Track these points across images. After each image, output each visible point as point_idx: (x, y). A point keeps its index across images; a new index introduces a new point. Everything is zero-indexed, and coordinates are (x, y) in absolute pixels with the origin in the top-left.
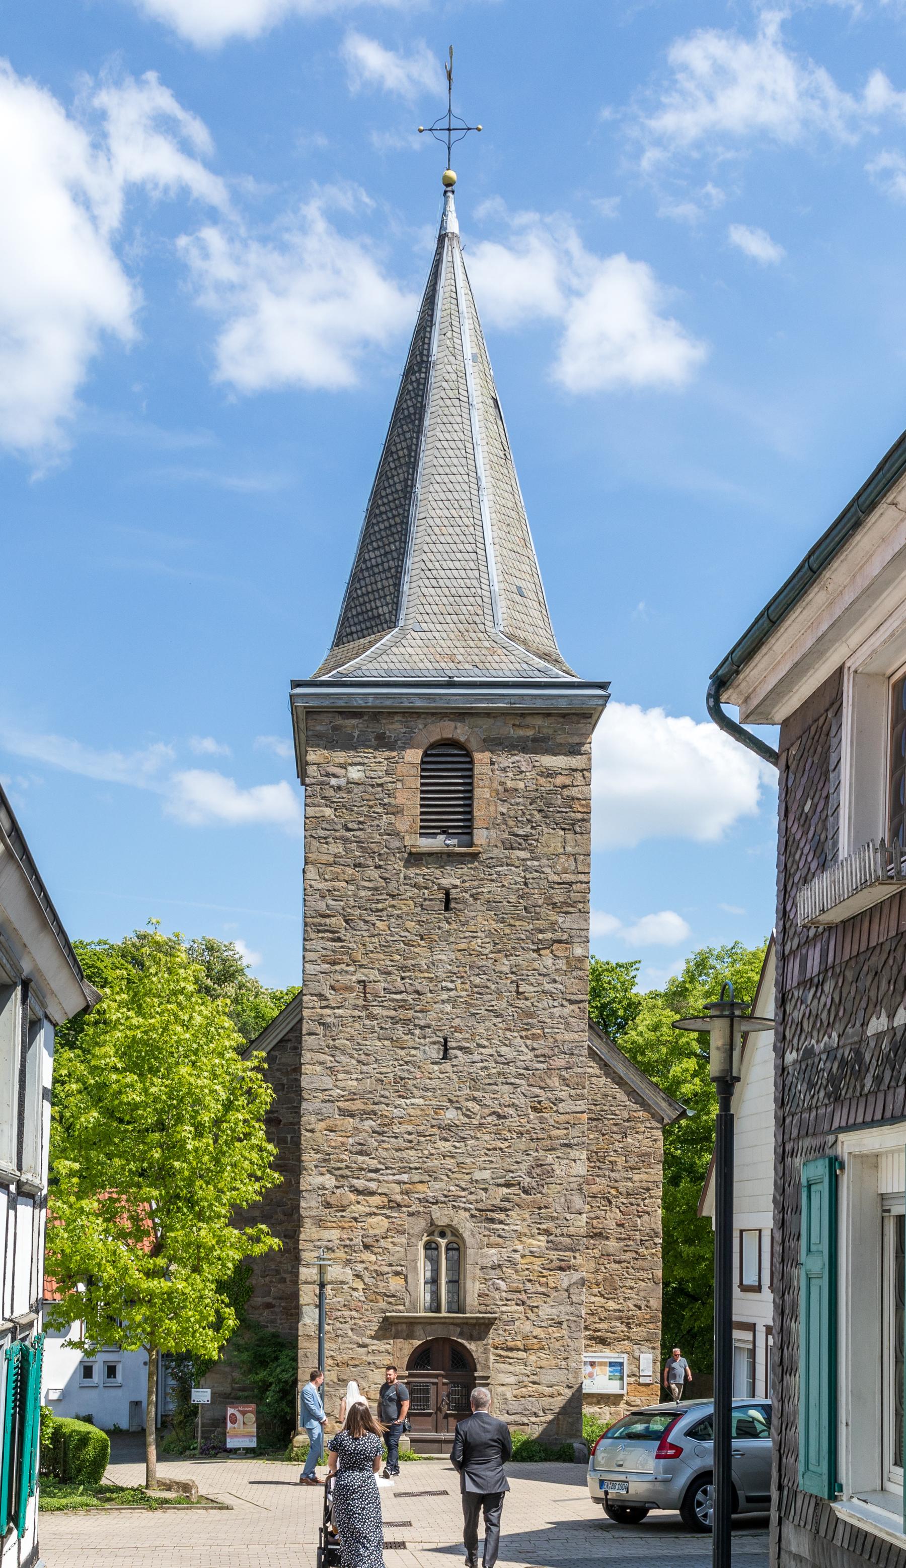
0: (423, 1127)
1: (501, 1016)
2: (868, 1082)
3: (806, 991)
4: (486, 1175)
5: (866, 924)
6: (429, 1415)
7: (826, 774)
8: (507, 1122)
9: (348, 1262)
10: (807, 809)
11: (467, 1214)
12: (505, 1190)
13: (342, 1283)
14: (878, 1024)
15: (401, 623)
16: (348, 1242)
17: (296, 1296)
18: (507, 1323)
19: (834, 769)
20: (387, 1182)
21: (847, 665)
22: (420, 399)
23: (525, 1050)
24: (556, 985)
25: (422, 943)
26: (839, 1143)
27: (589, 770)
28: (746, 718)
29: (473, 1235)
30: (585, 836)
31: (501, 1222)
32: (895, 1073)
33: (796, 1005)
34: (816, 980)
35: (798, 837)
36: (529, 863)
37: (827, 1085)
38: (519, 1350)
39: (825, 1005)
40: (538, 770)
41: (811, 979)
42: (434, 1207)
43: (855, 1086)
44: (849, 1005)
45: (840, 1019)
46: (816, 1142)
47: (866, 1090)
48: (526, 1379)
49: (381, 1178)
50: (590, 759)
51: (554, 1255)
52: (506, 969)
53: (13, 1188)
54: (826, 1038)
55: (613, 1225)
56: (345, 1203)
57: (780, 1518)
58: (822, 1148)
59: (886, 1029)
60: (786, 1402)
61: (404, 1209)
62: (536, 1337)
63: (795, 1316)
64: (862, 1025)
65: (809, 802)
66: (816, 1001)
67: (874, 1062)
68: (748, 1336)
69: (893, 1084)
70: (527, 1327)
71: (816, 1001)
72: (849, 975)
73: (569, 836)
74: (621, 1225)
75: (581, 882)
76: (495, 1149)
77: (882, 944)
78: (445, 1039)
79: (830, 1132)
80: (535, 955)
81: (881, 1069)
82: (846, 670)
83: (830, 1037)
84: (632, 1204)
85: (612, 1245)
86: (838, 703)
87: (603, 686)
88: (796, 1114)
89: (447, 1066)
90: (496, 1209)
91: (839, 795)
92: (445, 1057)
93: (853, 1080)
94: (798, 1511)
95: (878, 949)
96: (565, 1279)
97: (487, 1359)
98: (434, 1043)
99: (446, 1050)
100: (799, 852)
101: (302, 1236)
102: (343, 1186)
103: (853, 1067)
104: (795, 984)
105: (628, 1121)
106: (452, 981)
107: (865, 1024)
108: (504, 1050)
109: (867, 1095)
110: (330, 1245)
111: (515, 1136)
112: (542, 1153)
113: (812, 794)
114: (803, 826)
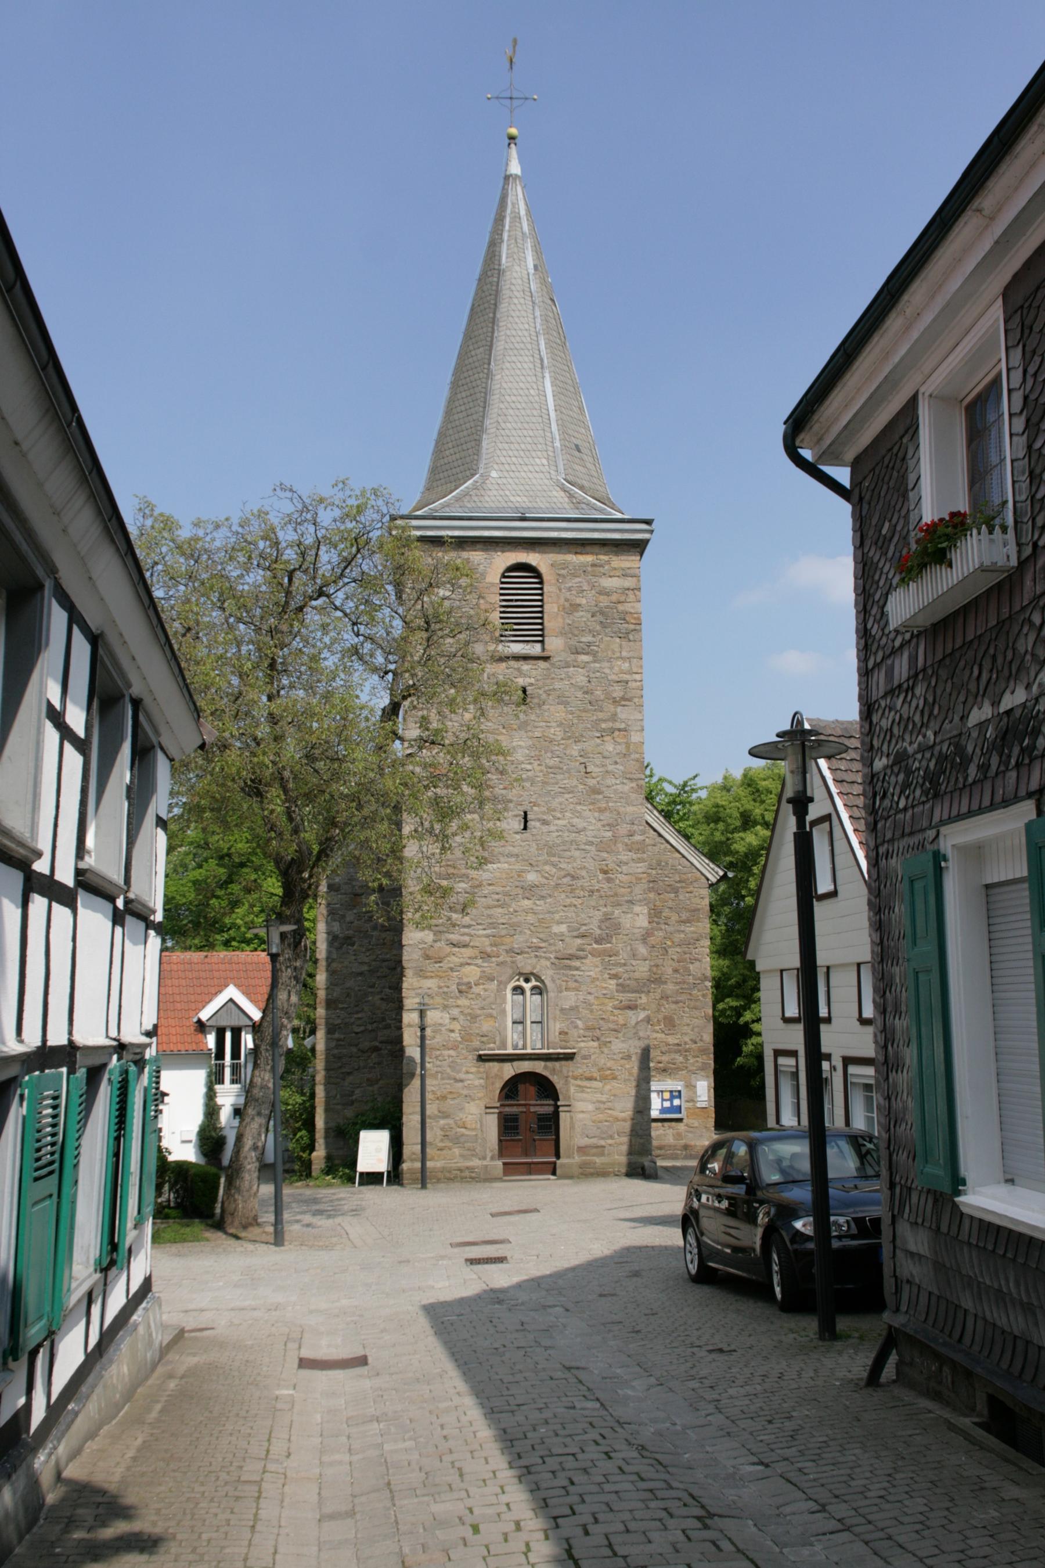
0: (508, 888)
1: (572, 792)
2: (972, 771)
3: (895, 699)
4: (563, 928)
5: (961, 621)
6: (520, 1140)
7: (905, 496)
8: (580, 883)
9: (445, 1007)
10: (884, 532)
11: (548, 963)
12: (579, 941)
13: (440, 1024)
14: (976, 716)
15: (481, 471)
16: (446, 990)
17: (399, 1039)
18: (585, 1057)
19: (913, 488)
20: (478, 936)
21: (922, 390)
22: (486, 366)
23: (594, 821)
24: (618, 766)
25: (504, 731)
26: (941, 837)
27: (639, 589)
29: (553, 981)
30: (638, 644)
31: (577, 969)
32: (1004, 758)
33: (883, 713)
34: (905, 686)
35: (875, 560)
36: (592, 665)
37: (924, 783)
38: (596, 1080)
39: (917, 707)
40: (598, 589)
41: (900, 686)
42: (519, 957)
43: (957, 779)
45: (936, 717)
47: (970, 780)
48: (602, 1106)
49: (473, 932)
50: (639, 581)
51: (622, 996)
52: (575, 753)
53: (120, 903)
54: (920, 738)
55: (670, 971)
56: (442, 955)
57: (893, 1216)
58: (921, 846)
59: (990, 716)
60: (893, 1099)
61: (494, 959)
62: (610, 1069)
64: (962, 718)
65: (887, 525)
66: (906, 706)
67: (978, 751)
68: (791, 1061)
69: (1002, 768)
70: (602, 1061)
71: (906, 706)
74: (676, 971)
75: (636, 681)
76: (570, 906)
77: (980, 636)
78: (525, 813)
79: (930, 827)
80: (598, 741)
81: (987, 756)
82: (920, 396)
83: (924, 736)
84: (685, 953)
85: (670, 987)
86: (915, 427)
87: (648, 522)
88: (889, 817)
89: (527, 835)
90: (570, 957)
91: (920, 510)
92: (525, 828)
93: (954, 773)
94: (914, 1209)
95: (976, 643)
96: (634, 1017)
97: (568, 1090)
98: (516, 816)
99: (526, 822)
100: (878, 573)
101: (405, 985)
102: (440, 940)
103: (954, 759)
104: (881, 694)
105: (680, 882)
106: (530, 763)
107: (964, 718)
108: (575, 821)
109: (971, 785)
110: (430, 992)
111: (587, 894)
112: (609, 909)
113: (889, 516)
114: (881, 548)
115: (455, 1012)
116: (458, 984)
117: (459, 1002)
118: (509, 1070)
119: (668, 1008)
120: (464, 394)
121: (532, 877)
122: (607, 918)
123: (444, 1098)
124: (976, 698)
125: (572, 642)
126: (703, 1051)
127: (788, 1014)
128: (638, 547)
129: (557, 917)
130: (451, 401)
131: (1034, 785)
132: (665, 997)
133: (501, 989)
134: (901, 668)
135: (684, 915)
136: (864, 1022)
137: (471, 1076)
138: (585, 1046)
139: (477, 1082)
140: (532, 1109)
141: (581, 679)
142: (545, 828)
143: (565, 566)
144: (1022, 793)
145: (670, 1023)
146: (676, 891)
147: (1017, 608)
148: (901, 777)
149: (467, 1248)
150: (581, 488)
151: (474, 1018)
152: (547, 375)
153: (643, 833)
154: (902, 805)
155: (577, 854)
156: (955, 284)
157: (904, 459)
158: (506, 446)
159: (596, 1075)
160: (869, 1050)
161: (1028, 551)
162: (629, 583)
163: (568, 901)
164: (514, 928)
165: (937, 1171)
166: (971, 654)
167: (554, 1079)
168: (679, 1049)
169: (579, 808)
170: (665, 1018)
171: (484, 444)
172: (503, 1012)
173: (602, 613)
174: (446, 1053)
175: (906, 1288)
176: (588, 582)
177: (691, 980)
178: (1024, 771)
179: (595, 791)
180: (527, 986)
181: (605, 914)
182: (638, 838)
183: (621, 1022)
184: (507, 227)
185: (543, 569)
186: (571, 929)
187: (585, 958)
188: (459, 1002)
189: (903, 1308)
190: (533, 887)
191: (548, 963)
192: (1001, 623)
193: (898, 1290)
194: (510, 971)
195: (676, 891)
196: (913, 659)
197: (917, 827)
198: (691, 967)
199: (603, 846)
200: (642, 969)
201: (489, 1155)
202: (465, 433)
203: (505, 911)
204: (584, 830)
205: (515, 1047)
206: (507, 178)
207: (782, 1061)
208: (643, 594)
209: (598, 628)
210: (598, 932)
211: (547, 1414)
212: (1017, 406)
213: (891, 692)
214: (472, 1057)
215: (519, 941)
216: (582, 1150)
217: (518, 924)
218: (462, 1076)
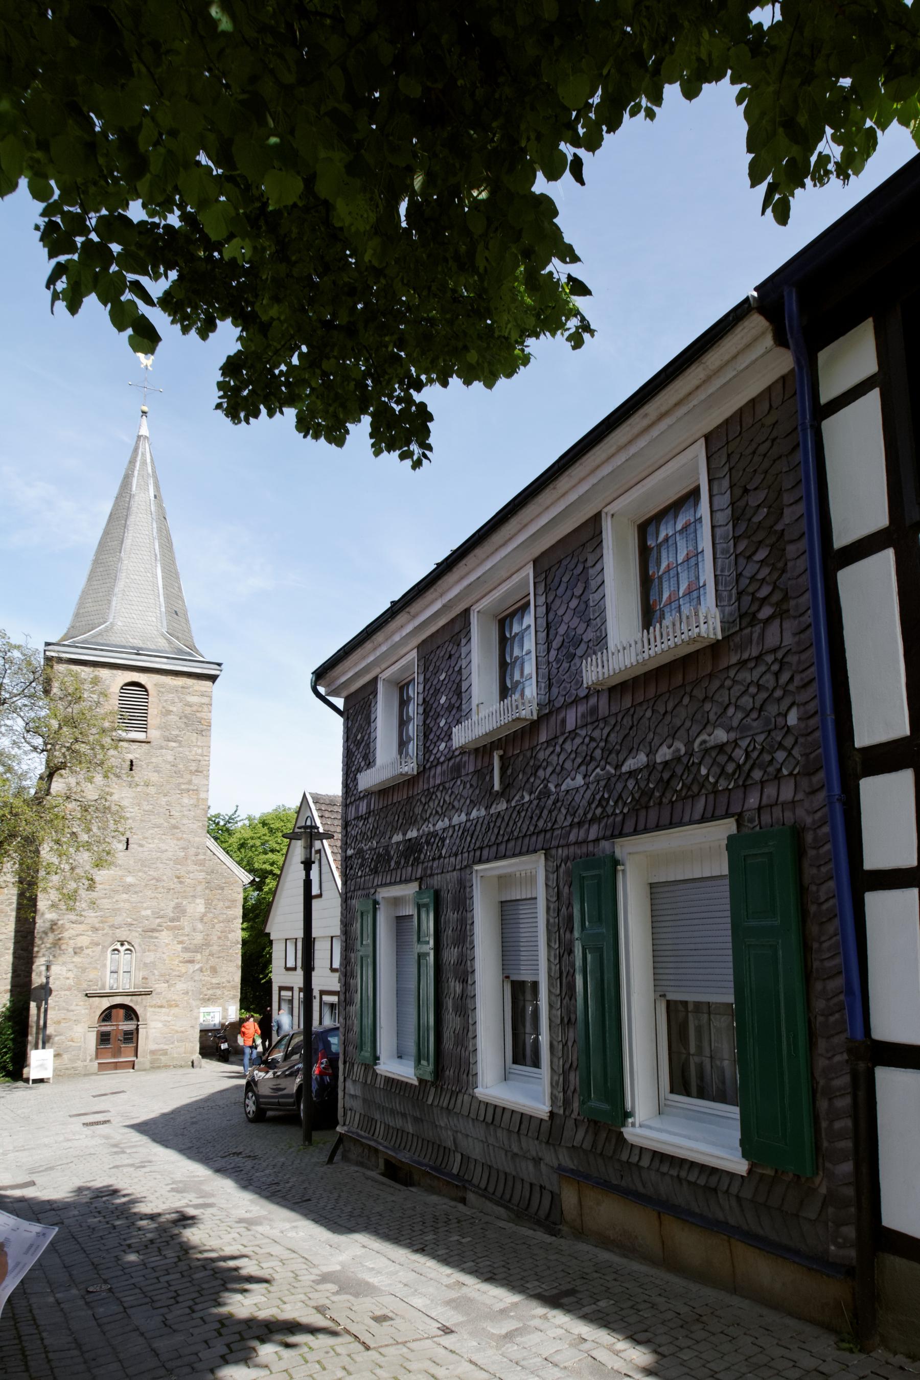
2: (393, 864)
7: (369, 724)
8: (162, 884)
10: (358, 738)
11: (137, 934)
12: (159, 920)
15: (111, 620)
27: (211, 705)
28: (328, 695)
29: (140, 945)
31: (156, 938)
44: (382, 828)
46: (365, 892)
52: (163, 803)
55: (215, 938)
58: (367, 895)
63: (353, 976)
68: (289, 993)
72: (382, 815)
73: (200, 737)
85: (215, 948)
87: (219, 665)
89: (127, 853)
90: (153, 930)
92: (127, 849)
96: (192, 968)
107: (390, 838)
115: (71, 966)
116: (74, 948)
117: (74, 960)
118: (106, 1003)
119: (213, 961)
120: (101, 569)
121: (130, 879)
122: (178, 907)
123: (59, 1022)
124: (395, 830)
125: (167, 734)
126: (234, 987)
127: (288, 966)
128: (213, 678)
129: (145, 905)
130: (93, 572)
131: (418, 876)
132: (211, 955)
133: (104, 949)
134: (363, 808)
135: (227, 904)
136: (333, 970)
137: (78, 1008)
138: (160, 987)
139: (83, 1012)
140: (120, 1028)
141: (170, 758)
142: (140, 849)
143: (163, 686)
144: (413, 878)
145: (214, 970)
146: (222, 889)
147: (415, 793)
148: (360, 860)
149: (82, 1117)
150: (177, 638)
151: (84, 970)
152: (159, 565)
153: (205, 854)
154: (360, 874)
155: (161, 865)
156: (397, 638)
157: (370, 706)
158: (128, 606)
159: (165, 1004)
160: (336, 987)
161: (422, 769)
162: (205, 700)
163: (153, 895)
164: (116, 911)
165: (367, 1054)
166: (395, 809)
167: (136, 1008)
168: (218, 986)
169: (163, 837)
170: (211, 967)
171: (114, 603)
172: (105, 966)
173: (186, 717)
174: (63, 993)
175: (349, 1113)
176: (179, 698)
177: (229, 943)
178: (415, 868)
179: (175, 827)
180: (122, 949)
181: (177, 904)
182: (201, 857)
183: (184, 971)
184: (137, 468)
185: (149, 687)
186: (153, 913)
187: (162, 931)
188: (74, 960)
189: (347, 1123)
190: (131, 885)
191: (137, 934)
192: (408, 798)
193: (345, 1115)
194: (111, 940)
195: (222, 889)
196: (369, 805)
197: (366, 886)
198: (230, 936)
199: (177, 861)
200: (198, 938)
201: (89, 1058)
202: (101, 594)
203: (109, 901)
204: (166, 851)
205: (111, 988)
206: (139, 437)
207: (283, 993)
208: (214, 708)
209: (183, 726)
210: (172, 915)
211: (157, 1194)
212: (421, 701)
213: (357, 818)
214: (81, 995)
215: (118, 920)
216: (153, 1052)
217: (119, 909)
218: (73, 1008)
